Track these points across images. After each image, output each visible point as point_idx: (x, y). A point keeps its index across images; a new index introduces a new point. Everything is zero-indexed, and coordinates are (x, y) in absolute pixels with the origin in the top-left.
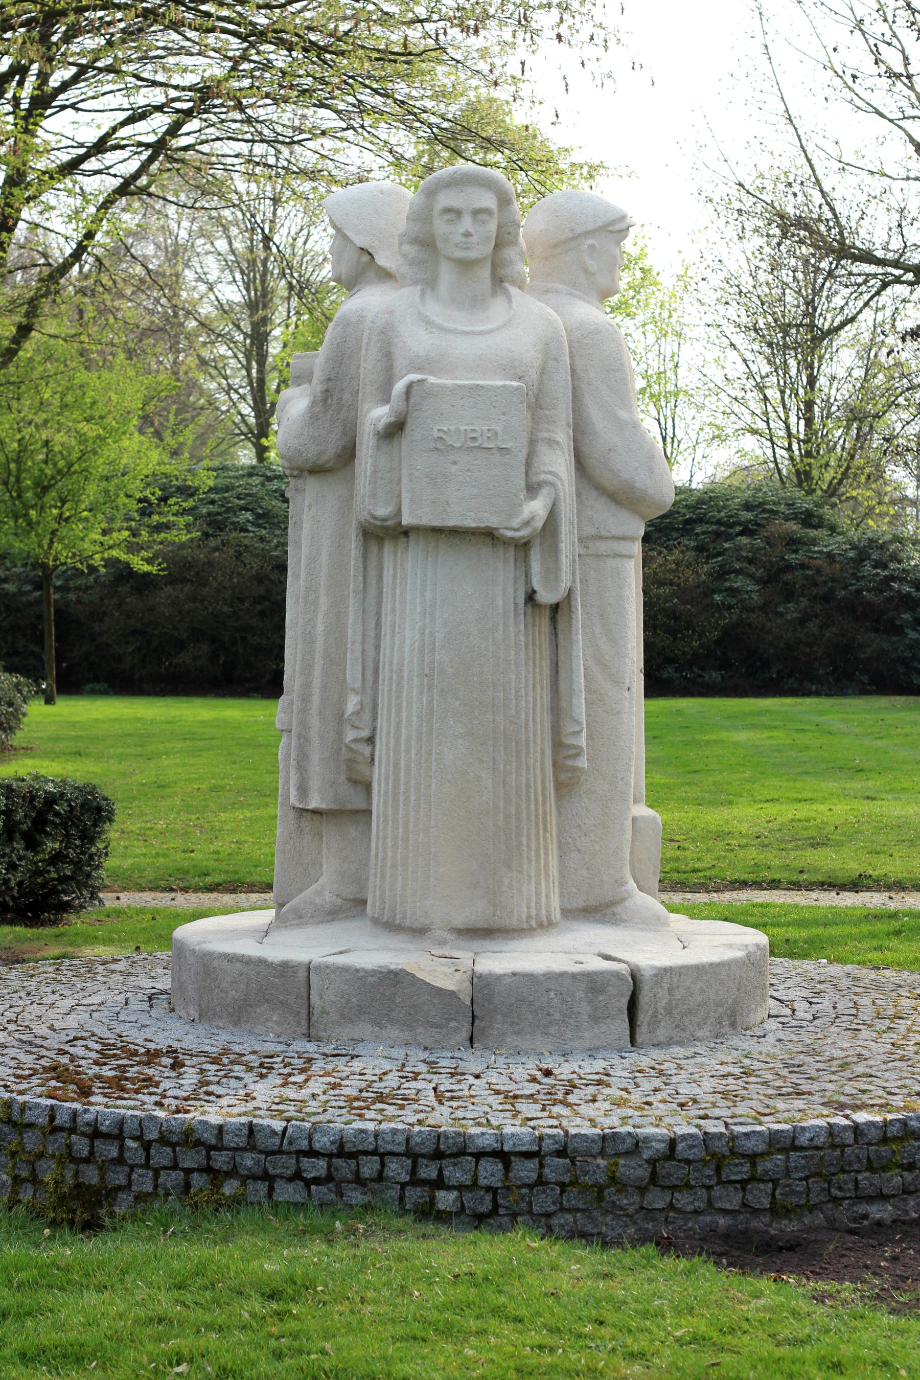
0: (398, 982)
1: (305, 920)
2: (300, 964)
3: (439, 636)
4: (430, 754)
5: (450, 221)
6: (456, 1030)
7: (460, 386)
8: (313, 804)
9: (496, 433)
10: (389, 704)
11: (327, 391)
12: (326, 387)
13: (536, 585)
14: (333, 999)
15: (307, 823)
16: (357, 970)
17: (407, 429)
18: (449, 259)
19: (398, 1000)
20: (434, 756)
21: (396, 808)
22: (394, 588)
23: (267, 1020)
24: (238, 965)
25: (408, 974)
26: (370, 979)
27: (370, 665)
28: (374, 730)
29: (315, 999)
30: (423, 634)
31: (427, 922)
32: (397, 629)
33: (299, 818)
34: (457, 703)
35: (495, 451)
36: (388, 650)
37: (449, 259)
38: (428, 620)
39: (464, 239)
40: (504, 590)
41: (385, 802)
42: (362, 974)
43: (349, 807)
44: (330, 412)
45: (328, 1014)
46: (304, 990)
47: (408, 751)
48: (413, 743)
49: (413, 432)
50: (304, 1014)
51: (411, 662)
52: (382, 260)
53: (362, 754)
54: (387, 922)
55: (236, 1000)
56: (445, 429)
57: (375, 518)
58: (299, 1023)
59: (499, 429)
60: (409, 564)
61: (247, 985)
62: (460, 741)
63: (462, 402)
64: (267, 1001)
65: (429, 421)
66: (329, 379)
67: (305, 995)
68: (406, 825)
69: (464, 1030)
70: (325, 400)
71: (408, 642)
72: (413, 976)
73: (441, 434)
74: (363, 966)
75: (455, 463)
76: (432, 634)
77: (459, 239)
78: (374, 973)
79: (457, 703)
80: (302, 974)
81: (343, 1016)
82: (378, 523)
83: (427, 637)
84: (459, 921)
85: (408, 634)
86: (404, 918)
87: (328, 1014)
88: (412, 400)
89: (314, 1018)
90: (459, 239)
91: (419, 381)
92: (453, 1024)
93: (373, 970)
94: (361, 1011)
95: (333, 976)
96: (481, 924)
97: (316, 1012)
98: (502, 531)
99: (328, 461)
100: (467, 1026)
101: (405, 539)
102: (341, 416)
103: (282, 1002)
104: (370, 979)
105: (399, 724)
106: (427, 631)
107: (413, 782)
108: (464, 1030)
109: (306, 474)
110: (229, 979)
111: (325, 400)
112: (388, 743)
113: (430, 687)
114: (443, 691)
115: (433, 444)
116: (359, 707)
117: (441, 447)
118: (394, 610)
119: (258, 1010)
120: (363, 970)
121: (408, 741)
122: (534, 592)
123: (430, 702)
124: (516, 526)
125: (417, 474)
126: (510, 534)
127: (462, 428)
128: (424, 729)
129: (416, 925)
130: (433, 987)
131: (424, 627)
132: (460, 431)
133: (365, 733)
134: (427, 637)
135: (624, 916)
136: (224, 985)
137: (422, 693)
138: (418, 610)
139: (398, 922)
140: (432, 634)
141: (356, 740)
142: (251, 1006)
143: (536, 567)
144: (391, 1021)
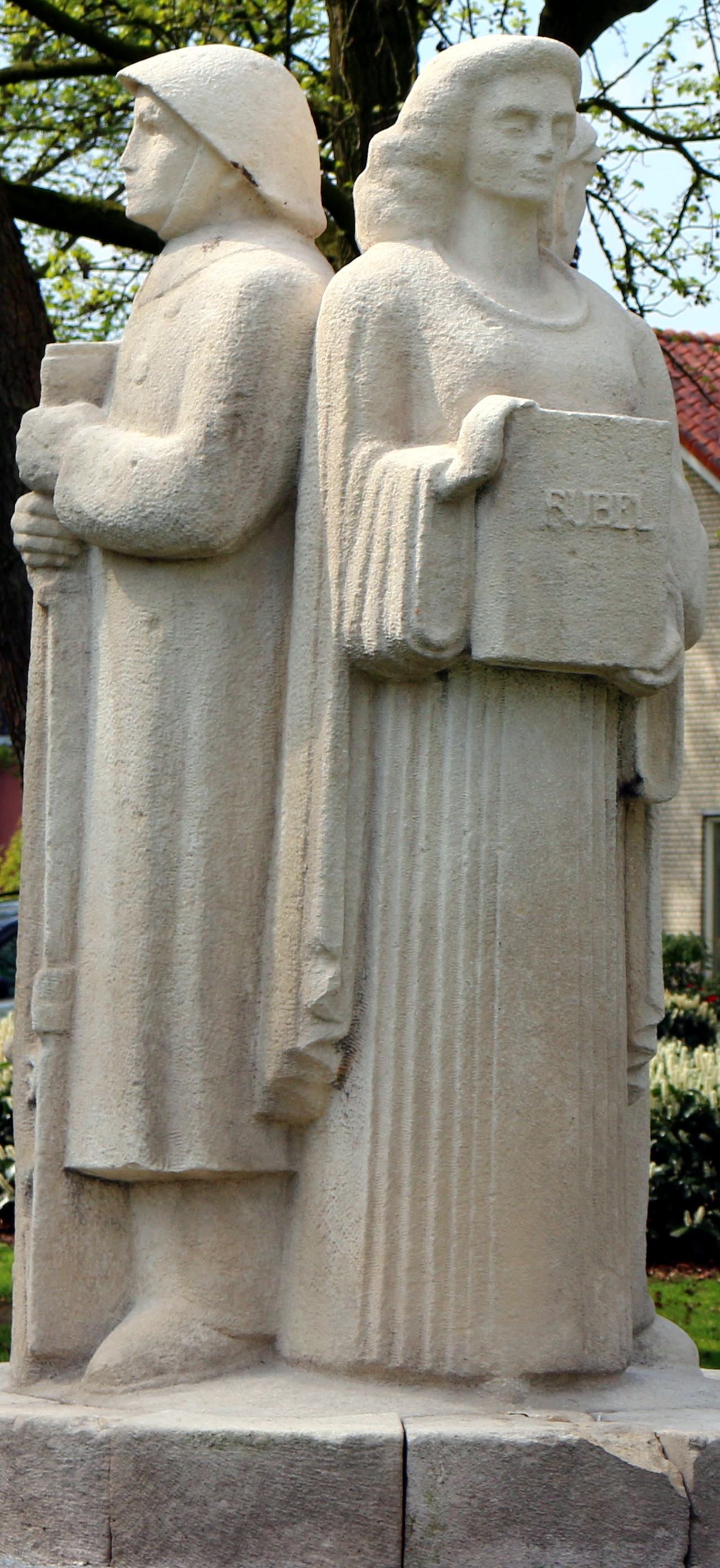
0: (575, 1463)
1: (170, 1377)
2: (389, 1441)
3: (503, 857)
4: (487, 1064)
5: (514, 132)
6: (666, 1543)
7: (582, 420)
8: (190, 1158)
9: (633, 504)
10: (404, 976)
11: (237, 415)
12: (232, 409)
13: (643, 768)
14: (457, 1500)
15: (92, 1201)
16: (502, 1446)
17: (501, 493)
18: (494, 196)
19: (574, 1495)
20: (495, 1068)
21: (420, 1162)
22: (412, 772)
23: (308, 1549)
24: (240, 1452)
25: (592, 1448)
26: (528, 1461)
27: (355, 907)
28: (355, 1023)
29: (417, 1502)
30: (475, 852)
31: (486, 1364)
32: (422, 843)
33: (77, 1194)
34: (530, 974)
35: (630, 535)
36: (399, 883)
37: (494, 196)
38: (485, 827)
39: (539, 165)
40: (595, 775)
41: (395, 1154)
42: (510, 1452)
43: (258, 1166)
44: (242, 454)
45: (444, 1528)
46: (396, 1487)
47: (447, 1060)
48: (458, 1045)
49: (512, 497)
50: (393, 1532)
51: (453, 901)
52: (270, 187)
53: (327, 1068)
54: (401, 1369)
55: (229, 1517)
56: (562, 492)
57: (426, 643)
58: (383, 1550)
59: (637, 496)
60: (449, 730)
61: (262, 1487)
62: (534, 1041)
63: (585, 447)
64: (310, 1514)
65: (538, 477)
66: (239, 395)
67: (398, 1496)
68: (443, 1193)
69: (677, 1542)
70: (232, 432)
71: (445, 865)
72: (601, 1451)
73: (556, 502)
74: (511, 1438)
75: (573, 553)
76: (491, 853)
77: (530, 163)
78: (532, 1449)
79: (530, 974)
80: (392, 1460)
81: (473, 1531)
82: (429, 654)
83: (483, 858)
84: (538, 1359)
85: (445, 851)
86: (440, 1358)
87: (444, 1528)
88: (513, 440)
89: (413, 1539)
90: (530, 163)
91: (524, 407)
92: (661, 1533)
93: (531, 1445)
94: (507, 1519)
95: (455, 1459)
96: (568, 1365)
97: (419, 1528)
98: (636, 673)
99: (227, 542)
100: (683, 1534)
101: (438, 684)
102: (260, 462)
103: (345, 1514)
104: (528, 1461)
105: (425, 1012)
106: (484, 846)
107: (458, 1114)
108: (677, 1542)
109: (96, 559)
110: (213, 1480)
111: (232, 432)
112: (400, 1046)
113: (489, 943)
114: (509, 952)
115: (544, 518)
116: (338, 983)
117: (555, 524)
118: (413, 809)
119: (287, 1532)
120: (514, 1445)
121: (448, 1043)
122: (638, 779)
123: (488, 972)
124: (659, 666)
125: (519, 569)
126: (648, 678)
127: (587, 493)
128: (478, 1020)
129: (465, 1369)
130: (632, 1469)
131: (476, 842)
132: (583, 498)
133: (340, 1031)
134: (483, 858)
135: (656, 1350)
136: (197, 1492)
137: (474, 956)
138: (468, 809)
139: (427, 1365)
140: (491, 853)
141: (320, 1044)
142: (269, 1525)
143: (642, 740)
144: (562, 1533)
